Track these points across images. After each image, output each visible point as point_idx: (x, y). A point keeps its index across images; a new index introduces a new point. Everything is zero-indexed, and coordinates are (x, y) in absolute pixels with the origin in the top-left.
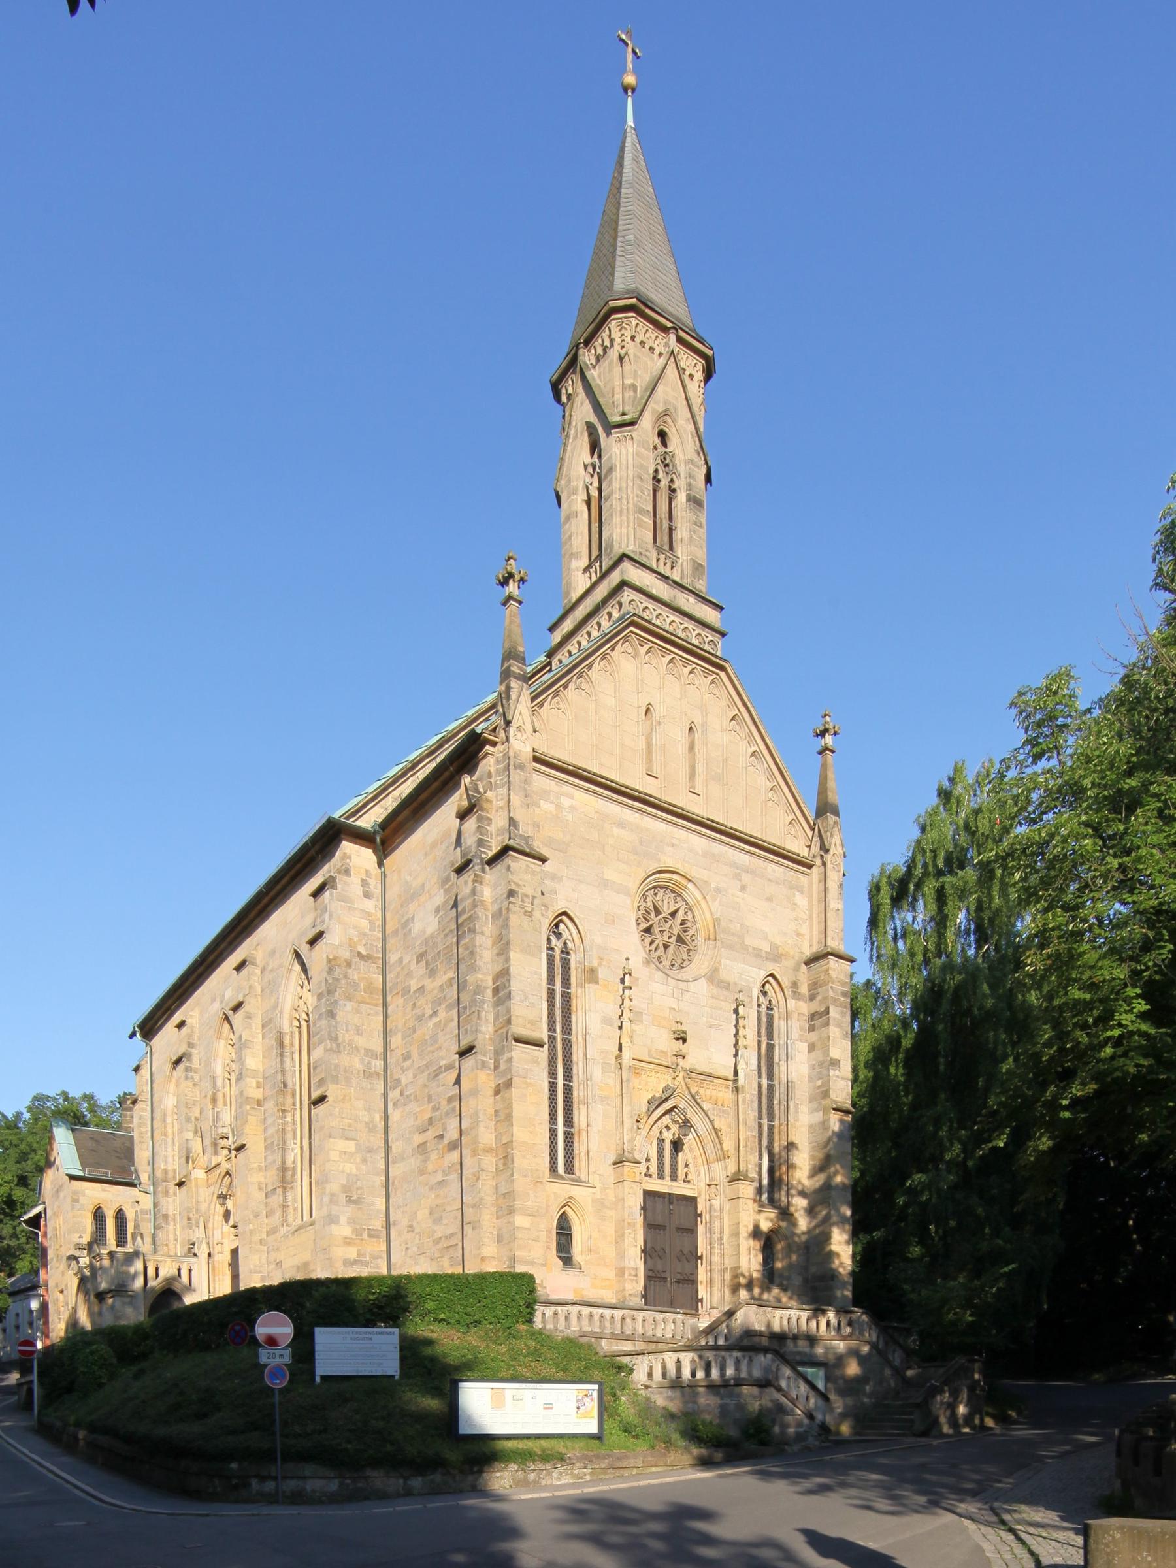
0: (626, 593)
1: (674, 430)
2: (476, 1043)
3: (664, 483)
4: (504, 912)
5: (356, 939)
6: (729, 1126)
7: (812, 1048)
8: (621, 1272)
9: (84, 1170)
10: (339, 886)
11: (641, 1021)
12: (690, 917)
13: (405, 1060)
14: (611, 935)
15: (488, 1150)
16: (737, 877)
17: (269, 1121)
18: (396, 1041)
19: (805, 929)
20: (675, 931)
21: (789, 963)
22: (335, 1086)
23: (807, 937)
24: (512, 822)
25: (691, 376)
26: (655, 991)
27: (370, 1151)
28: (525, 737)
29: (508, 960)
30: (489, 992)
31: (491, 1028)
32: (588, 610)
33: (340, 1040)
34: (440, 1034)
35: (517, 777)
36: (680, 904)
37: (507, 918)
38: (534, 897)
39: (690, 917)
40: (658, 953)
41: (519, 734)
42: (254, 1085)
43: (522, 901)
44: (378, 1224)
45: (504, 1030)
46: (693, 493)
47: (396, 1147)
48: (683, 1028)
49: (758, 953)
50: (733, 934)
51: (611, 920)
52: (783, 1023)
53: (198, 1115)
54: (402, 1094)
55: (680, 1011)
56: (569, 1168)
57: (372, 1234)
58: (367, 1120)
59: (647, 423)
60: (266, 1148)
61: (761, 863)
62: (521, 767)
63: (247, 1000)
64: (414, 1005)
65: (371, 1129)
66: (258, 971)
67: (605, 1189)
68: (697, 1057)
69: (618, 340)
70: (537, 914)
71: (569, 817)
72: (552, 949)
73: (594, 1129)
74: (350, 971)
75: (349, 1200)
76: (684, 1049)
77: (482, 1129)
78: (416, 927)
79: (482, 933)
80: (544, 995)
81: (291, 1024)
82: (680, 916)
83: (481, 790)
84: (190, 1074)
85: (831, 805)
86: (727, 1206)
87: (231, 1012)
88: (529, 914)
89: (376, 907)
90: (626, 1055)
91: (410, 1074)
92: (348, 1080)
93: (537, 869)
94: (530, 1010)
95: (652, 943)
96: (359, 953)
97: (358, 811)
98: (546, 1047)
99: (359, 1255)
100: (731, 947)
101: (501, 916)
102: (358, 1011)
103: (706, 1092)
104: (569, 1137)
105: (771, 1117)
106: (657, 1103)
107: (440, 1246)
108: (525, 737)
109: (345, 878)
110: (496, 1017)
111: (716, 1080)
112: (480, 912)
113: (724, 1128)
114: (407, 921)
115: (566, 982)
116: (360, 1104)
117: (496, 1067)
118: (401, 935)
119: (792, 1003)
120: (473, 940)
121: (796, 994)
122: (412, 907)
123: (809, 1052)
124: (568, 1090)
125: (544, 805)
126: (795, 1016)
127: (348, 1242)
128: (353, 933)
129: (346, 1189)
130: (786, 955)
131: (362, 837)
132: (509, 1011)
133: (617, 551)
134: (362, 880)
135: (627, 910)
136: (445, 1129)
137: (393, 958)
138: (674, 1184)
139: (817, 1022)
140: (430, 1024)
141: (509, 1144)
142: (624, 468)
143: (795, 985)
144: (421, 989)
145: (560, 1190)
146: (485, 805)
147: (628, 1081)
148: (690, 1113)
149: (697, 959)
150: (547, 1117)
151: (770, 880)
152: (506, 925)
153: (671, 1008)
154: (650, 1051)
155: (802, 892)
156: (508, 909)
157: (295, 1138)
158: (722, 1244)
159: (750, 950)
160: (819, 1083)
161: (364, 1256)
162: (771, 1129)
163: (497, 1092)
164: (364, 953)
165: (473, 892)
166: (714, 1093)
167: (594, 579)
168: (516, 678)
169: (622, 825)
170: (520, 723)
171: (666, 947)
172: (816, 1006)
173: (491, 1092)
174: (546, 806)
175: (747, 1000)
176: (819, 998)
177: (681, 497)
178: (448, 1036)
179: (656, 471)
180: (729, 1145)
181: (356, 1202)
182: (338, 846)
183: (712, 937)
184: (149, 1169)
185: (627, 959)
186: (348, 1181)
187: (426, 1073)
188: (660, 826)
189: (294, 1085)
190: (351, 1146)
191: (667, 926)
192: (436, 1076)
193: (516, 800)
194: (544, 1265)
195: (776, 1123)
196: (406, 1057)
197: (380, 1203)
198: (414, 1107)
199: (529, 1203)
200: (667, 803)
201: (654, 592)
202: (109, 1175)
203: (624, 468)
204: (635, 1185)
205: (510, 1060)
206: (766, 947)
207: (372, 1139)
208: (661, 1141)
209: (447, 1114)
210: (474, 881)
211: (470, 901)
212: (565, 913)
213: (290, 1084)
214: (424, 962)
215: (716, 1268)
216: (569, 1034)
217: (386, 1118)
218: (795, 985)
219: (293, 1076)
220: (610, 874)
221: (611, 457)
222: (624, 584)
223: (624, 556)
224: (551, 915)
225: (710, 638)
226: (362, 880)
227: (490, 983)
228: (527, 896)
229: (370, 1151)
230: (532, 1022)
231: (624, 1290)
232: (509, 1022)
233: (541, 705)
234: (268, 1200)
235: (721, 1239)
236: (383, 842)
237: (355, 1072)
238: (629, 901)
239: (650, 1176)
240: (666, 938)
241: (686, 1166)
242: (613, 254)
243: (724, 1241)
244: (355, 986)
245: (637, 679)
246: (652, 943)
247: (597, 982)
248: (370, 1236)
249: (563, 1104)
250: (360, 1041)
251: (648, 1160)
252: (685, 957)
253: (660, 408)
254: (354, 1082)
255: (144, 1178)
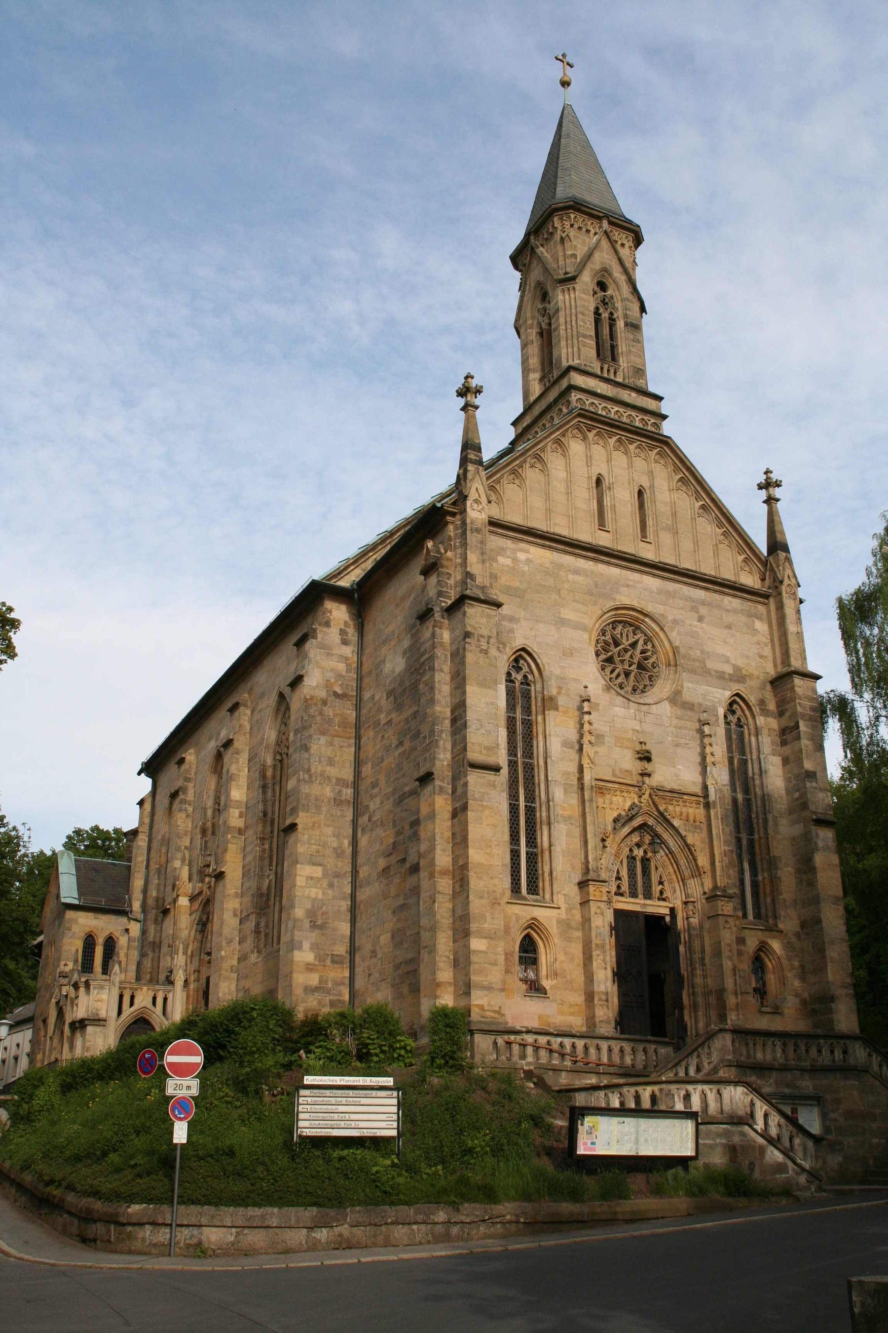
0: (573, 394)
1: (610, 280)
2: (433, 770)
3: (605, 315)
4: (461, 651)
5: (333, 680)
6: (702, 842)
7: (786, 761)
8: (590, 996)
9: (79, 899)
10: (319, 636)
11: (604, 743)
12: (649, 647)
13: (373, 787)
14: (572, 668)
15: (444, 873)
16: (694, 609)
17: (248, 849)
18: (367, 770)
19: (767, 652)
20: (636, 661)
21: (755, 683)
22: (305, 814)
23: (771, 658)
24: (468, 575)
25: (623, 245)
26: (616, 715)
27: (337, 875)
28: (480, 507)
29: (464, 693)
30: (447, 723)
31: (449, 756)
32: (543, 407)
33: (313, 770)
34: (405, 763)
35: (474, 539)
36: (639, 636)
37: (464, 657)
38: (489, 637)
39: (649, 647)
40: (620, 680)
41: (475, 506)
42: (237, 815)
43: (479, 641)
44: (342, 949)
45: (461, 756)
46: (629, 320)
47: (363, 872)
48: (647, 748)
49: (721, 676)
50: (694, 660)
51: (569, 653)
52: (753, 739)
53: (188, 844)
54: (370, 820)
55: (643, 732)
56: (533, 888)
57: (336, 960)
58: (335, 845)
59: (587, 279)
60: (243, 875)
61: (717, 596)
62: (478, 531)
63: (236, 737)
64: (383, 736)
65: (338, 853)
66: (248, 712)
67: (571, 909)
68: (664, 774)
69: (560, 228)
70: (493, 652)
71: (526, 568)
72: (512, 681)
73: (558, 849)
74: (325, 708)
75: (314, 926)
76: (649, 767)
77: (438, 851)
78: (388, 667)
79: (442, 670)
80: (503, 722)
81: (274, 759)
82: (640, 647)
83: (443, 551)
84: (184, 806)
85: (781, 543)
86: (707, 925)
87: (222, 749)
88: (486, 652)
89: (353, 652)
90: (587, 777)
91: (378, 801)
92: (318, 808)
93: (492, 613)
94: (488, 736)
95: (612, 672)
96: (335, 693)
97: (339, 573)
98: (505, 771)
99: (320, 982)
100: (692, 671)
101: (458, 657)
102: (331, 744)
103: (673, 810)
104: (532, 859)
105: (751, 832)
106: (623, 821)
107: (400, 972)
108: (480, 507)
109: (325, 629)
110: (454, 745)
111: (685, 797)
112: (439, 652)
113: (698, 843)
114: (379, 663)
115: (527, 710)
116: (329, 831)
117: (454, 792)
118: (373, 675)
119: (761, 720)
120: (433, 676)
121: (765, 712)
122: (384, 650)
123: (784, 765)
124: (531, 811)
125: (501, 559)
126: (765, 732)
127: (309, 968)
128: (330, 675)
129: (311, 914)
130: (751, 676)
131: (341, 595)
132: (465, 738)
133: (565, 364)
134: (341, 630)
135: (585, 645)
136: (407, 852)
137: (367, 695)
138: (648, 902)
139: (788, 737)
140: (397, 753)
141: (465, 867)
142: (568, 308)
143: (762, 702)
144: (389, 722)
145: (522, 913)
146: (445, 563)
147: (591, 800)
148: (659, 829)
149: (659, 683)
150: (507, 837)
151: (727, 610)
152: (463, 663)
153: (633, 730)
154: (613, 771)
155: (760, 619)
156: (464, 649)
157: (271, 865)
158: (704, 965)
159: (713, 673)
160: (797, 795)
161: (326, 982)
162: (751, 843)
163: (454, 815)
164: (340, 692)
165: (433, 635)
166: (684, 809)
167: (547, 384)
168: (471, 462)
169: (577, 572)
170: (476, 496)
171: (627, 674)
172: (786, 721)
173: (448, 816)
174: (504, 561)
175: (712, 719)
176: (788, 714)
177: (620, 324)
178: (411, 765)
179: (597, 309)
180: (703, 861)
181: (321, 927)
182: (341, 603)
183: (672, 663)
184: (141, 897)
185: (586, 687)
186: (313, 906)
187: (391, 800)
188: (615, 571)
189: (273, 813)
190: (318, 872)
191: (630, 654)
192: (400, 802)
193: (472, 557)
194: (502, 990)
195: (756, 836)
196: (374, 785)
197: (345, 928)
198: (380, 832)
199: (486, 925)
200: (619, 551)
201: (599, 391)
202: (103, 903)
203: (568, 308)
204: (602, 905)
205: (466, 784)
206: (728, 669)
207: (340, 864)
208: (632, 859)
209: (410, 838)
210: (434, 626)
211: (430, 643)
212: (523, 649)
213: (270, 813)
214: (392, 698)
215: (699, 990)
216: (531, 757)
217: (354, 843)
218: (762, 702)
219: (273, 805)
220: (567, 613)
221: (557, 302)
222: (571, 388)
223: (570, 368)
224: (509, 651)
225: (653, 421)
226: (341, 630)
227: (448, 714)
228: (483, 636)
229: (337, 875)
230: (488, 749)
231: (594, 1016)
232: (465, 749)
233: (498, 481)
234: (242, 926)
235: (703, 959)
236: (361, 598)
237: (325, 800)
238: (586, 636)
239: (622, 895)
240: (626, 667)
241: (661, 883)
242: (556, 177)
243: (707, 961)
244: (329, 721)
245: (587, 456)
246: (612, 672)
247: (557, 709)
248: (333, 962)
249: (526, 824)
250: (333, 772)
251: (618, 878)
252: (648, 683)
253: (598, 267)
254: (324, 809)
255: (136, 906)
